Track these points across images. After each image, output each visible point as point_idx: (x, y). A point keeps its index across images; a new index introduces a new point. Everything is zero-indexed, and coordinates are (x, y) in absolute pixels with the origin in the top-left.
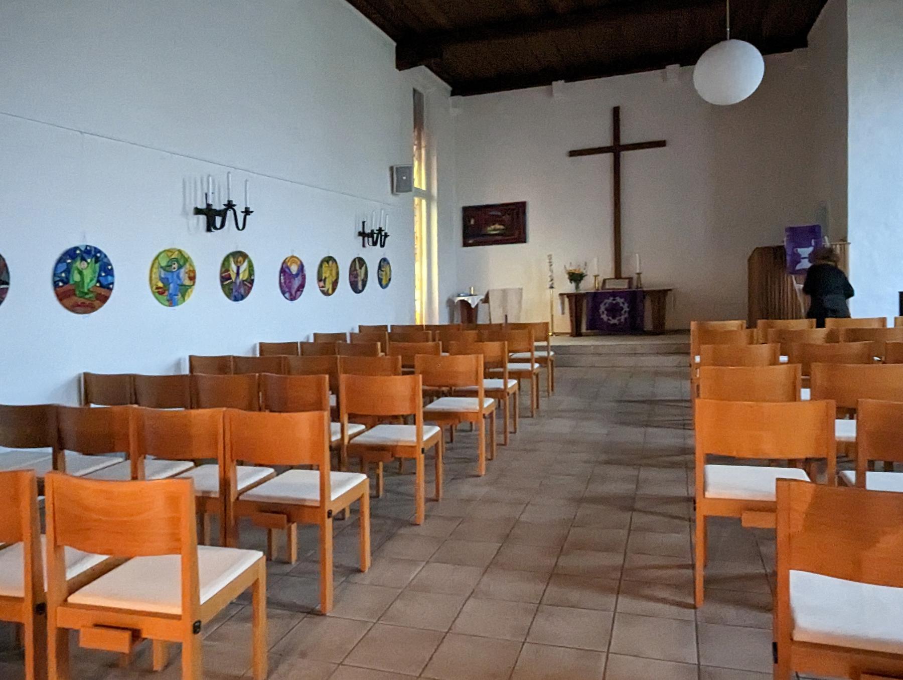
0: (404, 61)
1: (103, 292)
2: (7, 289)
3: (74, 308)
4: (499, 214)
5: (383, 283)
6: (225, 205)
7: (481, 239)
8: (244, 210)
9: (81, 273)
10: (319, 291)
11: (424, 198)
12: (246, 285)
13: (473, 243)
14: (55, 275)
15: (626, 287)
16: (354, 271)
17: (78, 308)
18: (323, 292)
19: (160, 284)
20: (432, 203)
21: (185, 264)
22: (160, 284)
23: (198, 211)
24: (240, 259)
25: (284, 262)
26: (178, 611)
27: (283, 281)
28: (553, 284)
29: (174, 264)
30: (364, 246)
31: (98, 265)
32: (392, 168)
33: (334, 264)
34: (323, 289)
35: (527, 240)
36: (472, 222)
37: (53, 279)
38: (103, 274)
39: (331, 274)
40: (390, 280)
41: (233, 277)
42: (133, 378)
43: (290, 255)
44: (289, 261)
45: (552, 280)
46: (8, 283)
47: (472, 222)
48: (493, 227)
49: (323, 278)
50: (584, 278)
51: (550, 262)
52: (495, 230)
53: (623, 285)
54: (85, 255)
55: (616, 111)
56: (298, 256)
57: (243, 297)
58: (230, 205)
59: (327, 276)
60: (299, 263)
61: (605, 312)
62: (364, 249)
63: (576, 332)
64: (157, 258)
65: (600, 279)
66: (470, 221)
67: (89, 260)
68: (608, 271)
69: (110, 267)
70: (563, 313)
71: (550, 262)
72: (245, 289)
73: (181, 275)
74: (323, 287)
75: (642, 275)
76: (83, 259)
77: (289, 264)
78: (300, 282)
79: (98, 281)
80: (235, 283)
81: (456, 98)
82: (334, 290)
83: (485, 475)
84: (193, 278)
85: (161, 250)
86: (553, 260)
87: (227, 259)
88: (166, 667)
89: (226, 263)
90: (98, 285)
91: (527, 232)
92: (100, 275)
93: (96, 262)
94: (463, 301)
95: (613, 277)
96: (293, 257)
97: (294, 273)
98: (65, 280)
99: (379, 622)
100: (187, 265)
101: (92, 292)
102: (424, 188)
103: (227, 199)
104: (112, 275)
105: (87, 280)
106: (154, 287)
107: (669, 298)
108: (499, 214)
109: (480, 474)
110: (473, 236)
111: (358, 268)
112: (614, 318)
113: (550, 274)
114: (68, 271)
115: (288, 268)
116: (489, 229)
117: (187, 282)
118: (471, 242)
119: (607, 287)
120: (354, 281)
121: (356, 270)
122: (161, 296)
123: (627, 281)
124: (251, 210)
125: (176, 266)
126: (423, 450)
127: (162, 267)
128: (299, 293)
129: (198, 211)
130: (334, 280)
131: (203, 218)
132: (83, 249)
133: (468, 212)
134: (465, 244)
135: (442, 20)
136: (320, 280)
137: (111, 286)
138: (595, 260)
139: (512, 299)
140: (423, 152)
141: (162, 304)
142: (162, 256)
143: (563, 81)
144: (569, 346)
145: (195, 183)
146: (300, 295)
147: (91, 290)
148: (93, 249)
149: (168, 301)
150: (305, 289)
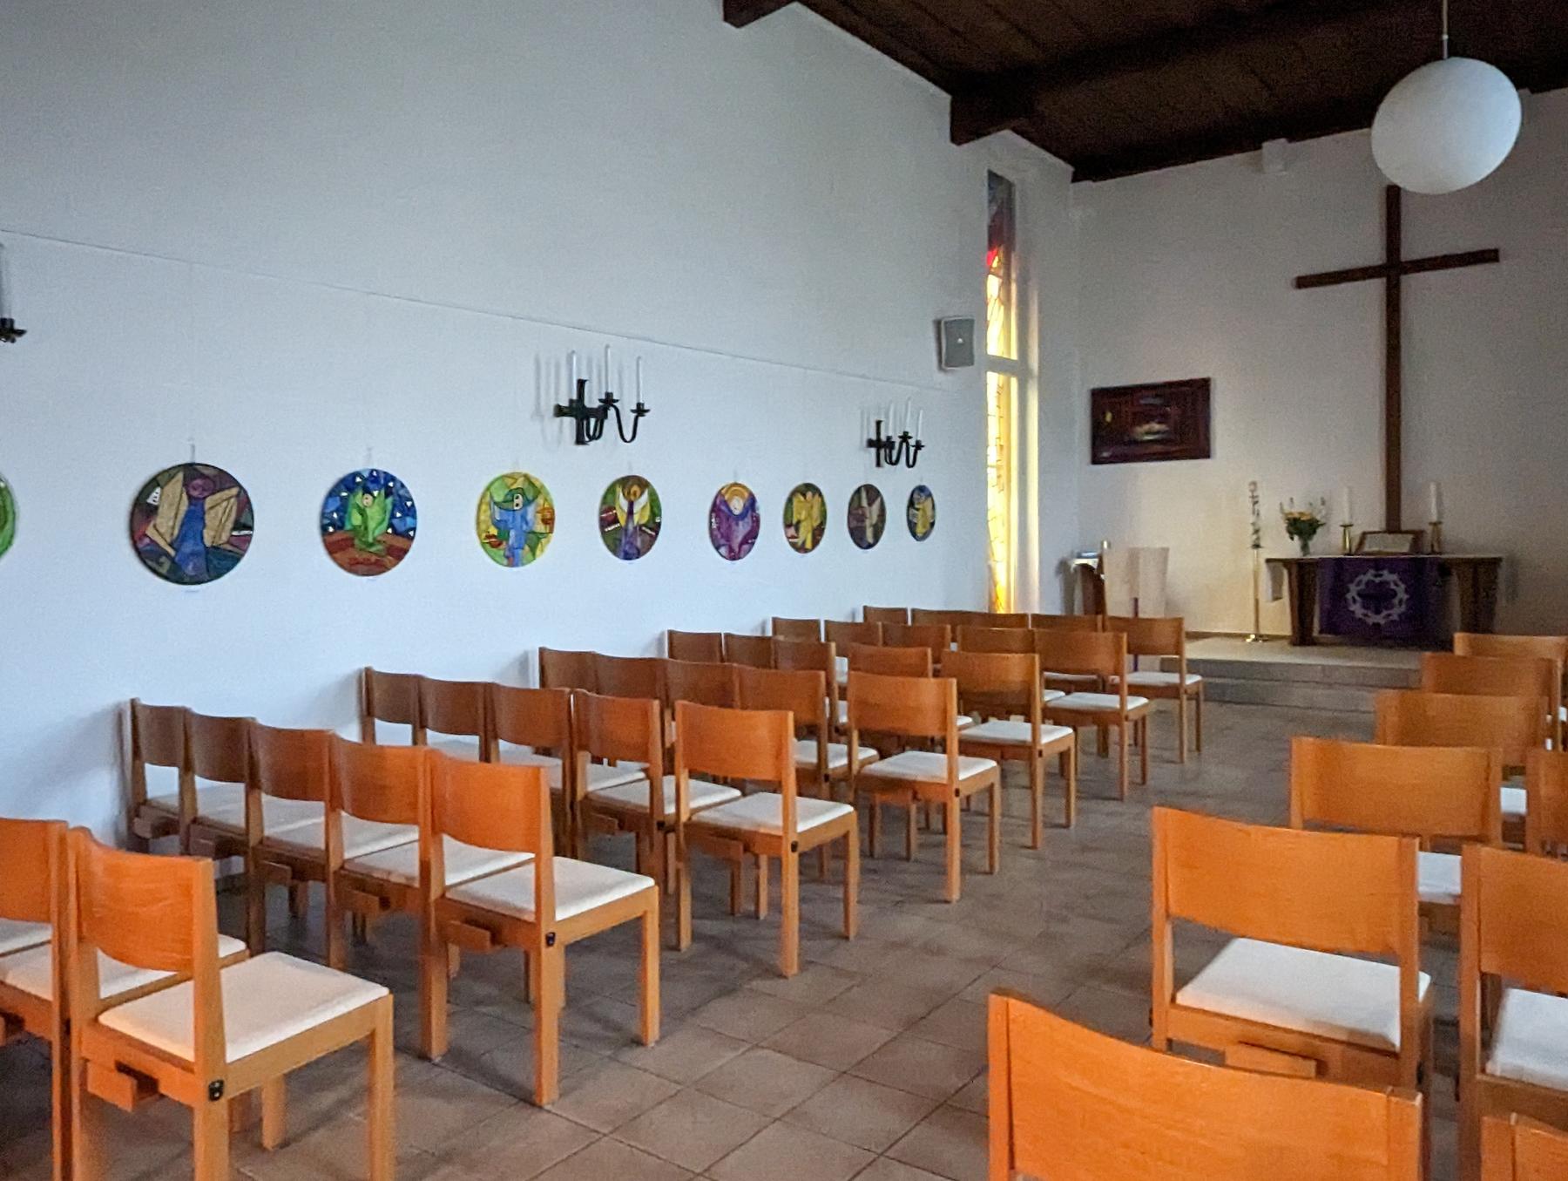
0: (965, 128)
1: (399, 542)
2: (251, 536)
3: (353, 566)
5: (919, 529)
6: (600, 400)
8: (635, 408)
9: (362, 512)
10: (787, 544)
11: (1014, 374)
12: (645, 532)
13: (1111, 456)
14: (323, 515)
15: (1406, 549)
16: (857, 509)
17: (359, 566)
18: (793, 545)
19: (494, 531)
20: (1029, 385)
21: (535, 498)
22: (494, 531)
24: (635, 488)
25: (720, 493)
26: (188, 1054)
27: (714, 526)
28: (1258, 539)
29: (517, 498)
30: (878, 464)
31: (390, 500)
32: (938, 323)
33: (817, 496)
34: (795, 540)
35: (1212, 453)
36: (1109, 417)
37: (321, 521)
38: (398, 515)
39: (809, 515)
40: (932, 524)
41: (622, 518)
42: (418, 679)
43: (732, 482)
44: (727, 492)
45: (1257, 531)
46: (251, 528)
47: (1109, 417)
48: (1146, 427)
49: (795, 521)
50: (1319, 530)
51: (1253, 497)
52: (1148, 433)
53: (1400, 546)
54: (371, 486)
56: (745, 484)
57: (639, 554)
58: (609, 401)
59: (803, 517)
60: (746, 495)
62: (880, 469)
63: (1302, 637)
64: (488, 489)
65: (1356, 532)
66: (1104, 414)
67: (376, 493)
68: (1371, 515)
69: (409, 504)
70: (1277, 598)
72: (643, 541)
73: (530, 516)
74: (793, 537)
75: (1443, 527)
76: (367, 491)
77: (726, 497)
78: (748, 528)
79: (391, 525)
80: (626, 530)
81: (1077, 184)
82: (816, 543)
83: (958, 901)
84: (549, 521)
85: (491, 479)
87: (611, 490)
88: (285, 1144)
89: (610, 496)
90: (390, 531)
91: (1212, 436)
92: (393, 516)
93: (387, 495)
94: (1085, 566)
96: (736, 484)
97: (737, 512)
98: (339, 523)
99: (614, 1136)
100: (540, 500)
101: (379, 542)
102: (1014, 356)
103: (604, 391)
104: (414, 516)
105: (372, 524)
106: (484, 535)
107: (1503, 573)
108: (1157, 401)
109: (948, 898)
111: (864, 503)
112: (1378, 612)
113: (1252, 519)
114: (343, 509)
115: (726, 503)
117: (540, 528)
118: (1105, 454)
119: (1366, 549)
120: (857, 528)
121: (860, 506)
122: (494, 550)
123: (1410, 537)
124: (646, 408)
125: (520, 500)
126: (794, 847)
127: (495, 503)
128: (745, 547)
129: (560, 412)
130: (816, 524)
131: (569, 423)
132: (366, 475)
133: (1102, 399)
134: (1096, 460)
135: (1022, 48)
136: (788, 525)
137: (411, 533)
139: (1148, 570)
140: (1014, 287)
141: (498, 562)
142: (496, 484)
143: (1283, 140)
144: (1270, 664)
145: (558, 366)
146: (750, 550)
147: (379, 538)
148: (382, 475)
149: (507, 557)
150: (758, 541)
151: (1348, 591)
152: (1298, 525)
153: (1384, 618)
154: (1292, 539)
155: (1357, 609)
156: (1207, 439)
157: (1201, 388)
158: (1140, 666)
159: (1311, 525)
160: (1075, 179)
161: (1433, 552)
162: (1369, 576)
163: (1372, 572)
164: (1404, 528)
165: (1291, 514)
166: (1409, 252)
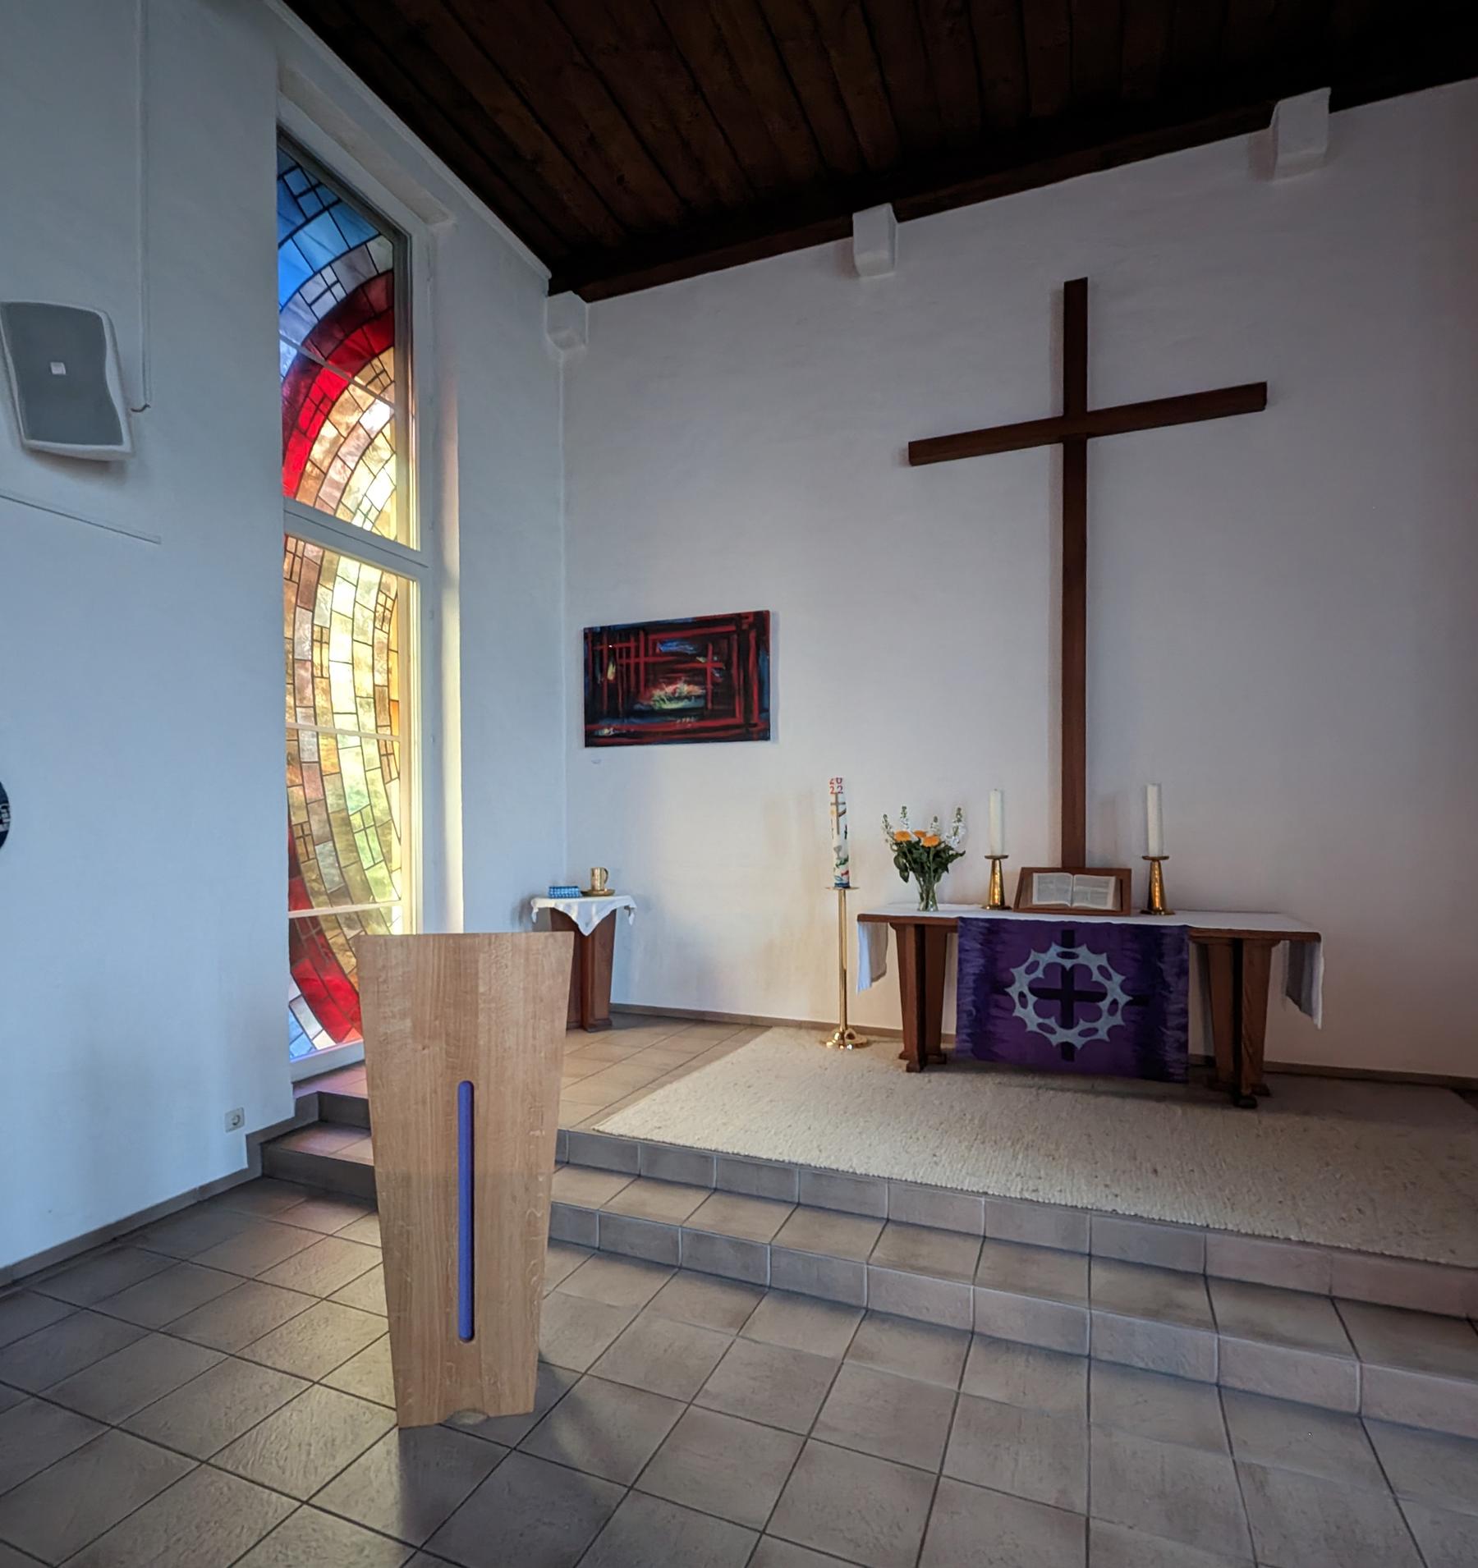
4: (689, 649)
7: (635, 724)
23: (987, 857)
36: (611, 672)
47: (611, 672)
48: (669, 689)
51: (837, 804)
55: (1075, 296)
61: (1032, 999)
65: (1011, 868)
66: (604, 671)
68: (1043, 848)
70: (877, 974)
71: (837, 804)
86: (850, 797)
95: (1058, 864)
108: (689, 649)
110: (614, 714)
112: (1067, 1022)
113: (836, 841)
116: (657, 693)
129: (987, 857)
134: (592, 739)
138: (994, 800)
151: (1011, 983)
152: (916, 854)
153: (1082, 1034)
154: (906, 879)
155: (1029, 1016)
156: (764, 710)
157: (759, 623)
158: (541, 1364)
159: (937, 854)
160: (554, 289)
161: (1150, 910)
162: (1052, 954)
163: (1055, 949)
164: (1088, 864)
165: (903, 834)
166: (1102, 396)
